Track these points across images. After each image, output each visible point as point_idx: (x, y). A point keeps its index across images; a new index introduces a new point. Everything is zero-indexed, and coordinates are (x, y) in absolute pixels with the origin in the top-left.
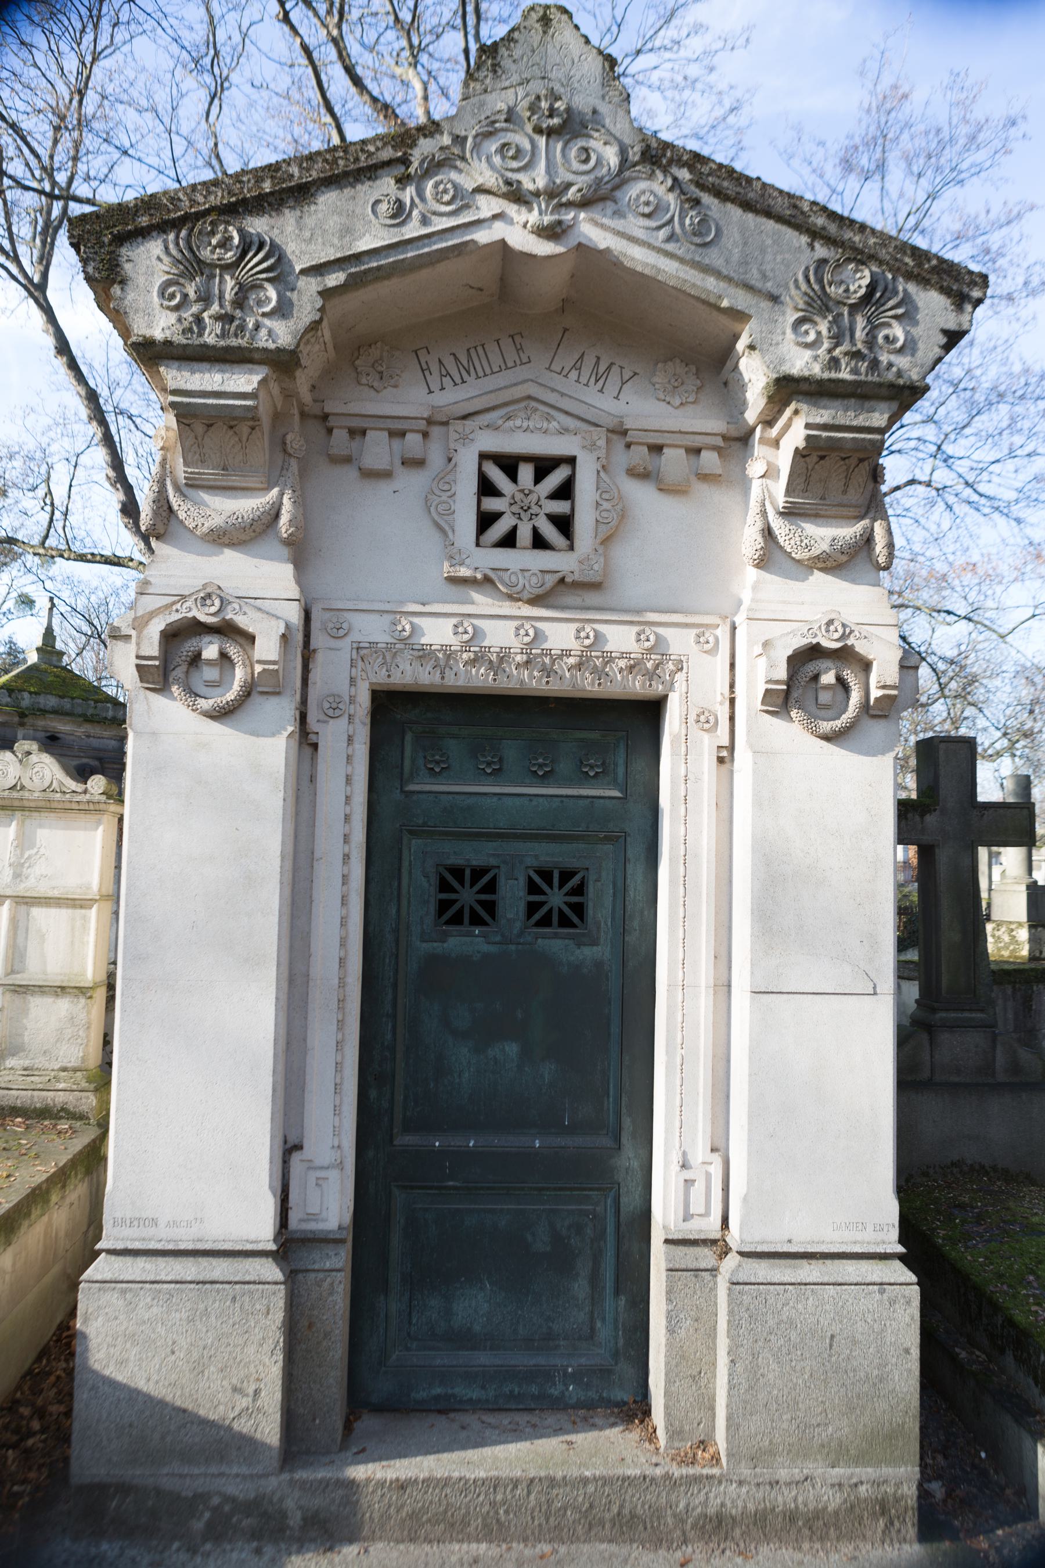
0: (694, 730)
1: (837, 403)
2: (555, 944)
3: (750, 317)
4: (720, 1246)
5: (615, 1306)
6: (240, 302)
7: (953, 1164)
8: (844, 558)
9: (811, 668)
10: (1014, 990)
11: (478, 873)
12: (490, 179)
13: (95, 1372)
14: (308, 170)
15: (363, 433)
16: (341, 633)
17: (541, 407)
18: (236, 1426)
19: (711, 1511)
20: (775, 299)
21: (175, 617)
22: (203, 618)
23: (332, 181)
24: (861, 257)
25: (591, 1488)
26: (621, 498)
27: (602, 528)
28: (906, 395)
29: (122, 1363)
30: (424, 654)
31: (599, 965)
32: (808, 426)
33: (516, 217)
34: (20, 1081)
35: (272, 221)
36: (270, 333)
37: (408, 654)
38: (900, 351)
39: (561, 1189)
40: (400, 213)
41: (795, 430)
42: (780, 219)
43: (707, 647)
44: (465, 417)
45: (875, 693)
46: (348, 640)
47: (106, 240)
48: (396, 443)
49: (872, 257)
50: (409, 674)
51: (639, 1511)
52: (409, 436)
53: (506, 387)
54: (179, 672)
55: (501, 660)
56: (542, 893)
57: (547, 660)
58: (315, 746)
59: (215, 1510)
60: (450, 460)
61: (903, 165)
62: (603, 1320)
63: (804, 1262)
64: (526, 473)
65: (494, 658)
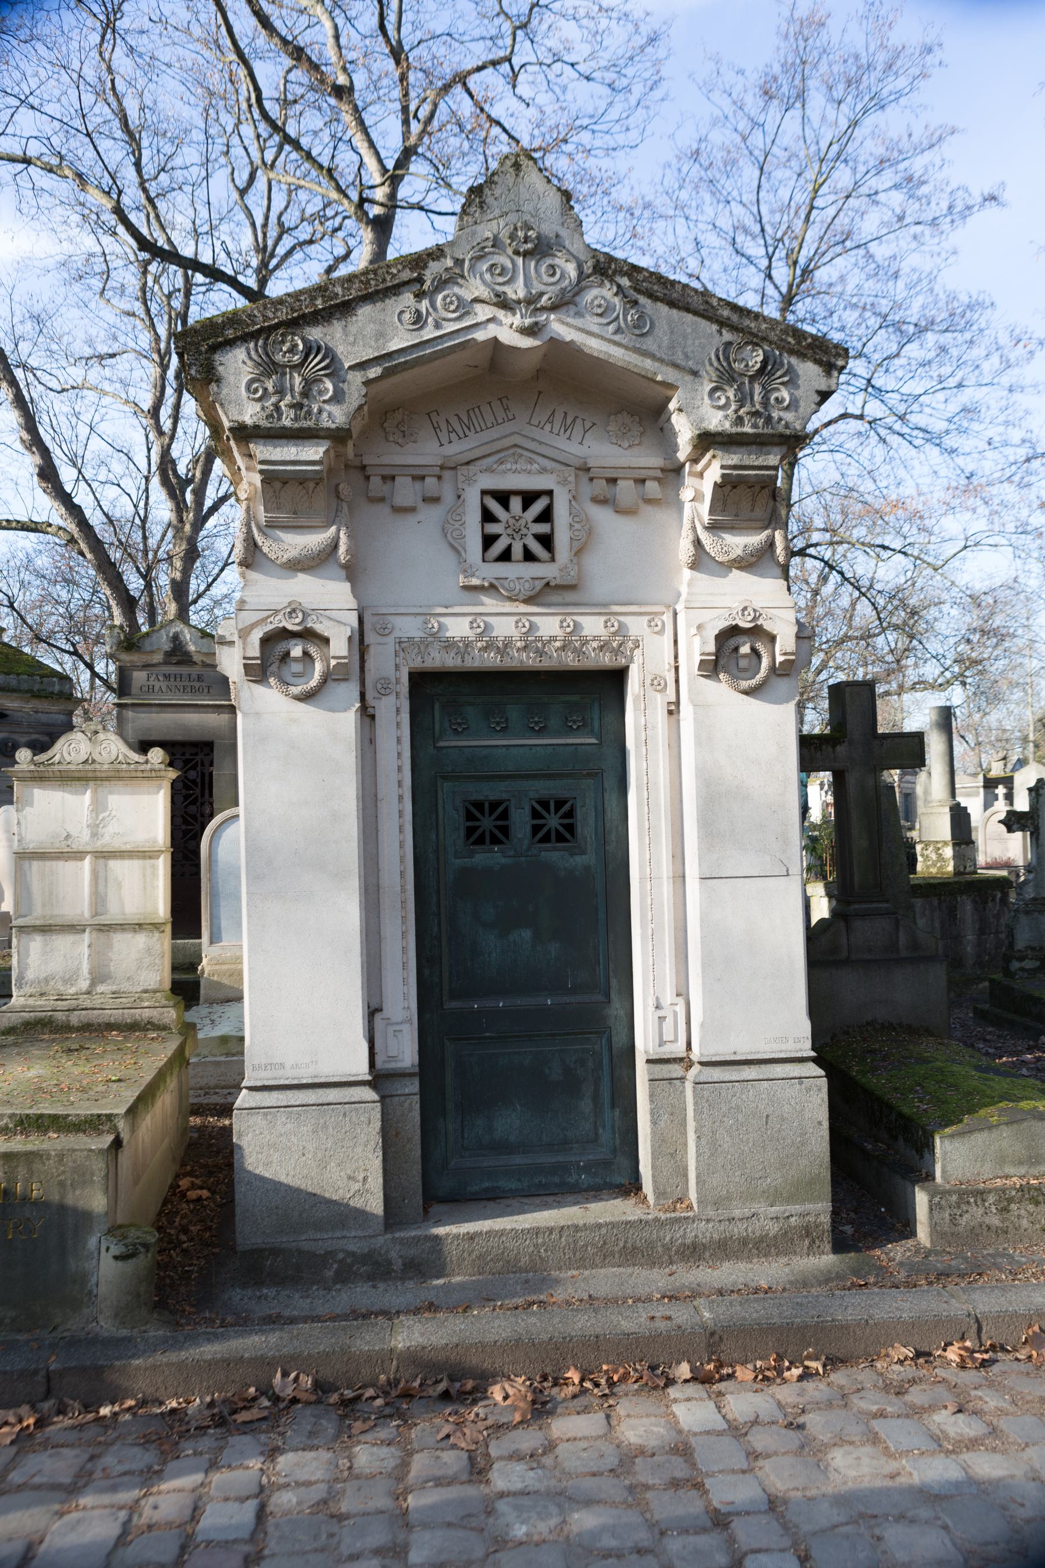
0: (650, 692)
1: (743, 449)
2: (555, 856)
3: (677, 388)
4: (685, 1062)
5: (612, 1116)
6: (306, 393)
7: (868, 1023)
8: (754, 559)
9: (732, 642)
10: (940, 903)
11: (494, 805)
12: (483, 292)
13: (249, 1172)
14: (349, 289)
15: (393, 478)
16: (387, 631)
17: (525, 453)
18: (351, 1203)
19: (688, 1241)
20: (695, 373)
21: (270, 627)
22: (290, 627)
23: (368, 298)
24: (755, 340)
25: (604, 1231)
26: (587, 520)
27: (575, 543)
28: (793, 443)
29: (268, 1164)
30: (449, 645)
31: (587, 868)
32: (723, 467)
33: (504, 320)
34: (110, 1003)
35: (325, 330)
36: (330, 415)
37: (437, 645)
38: (787, 408)
39: (568, 1034)
40: (419, 320)
41: (714, 469)
42: (696, 313)
43: (657, 629)
44: (468, 463)
45: (779, 659)
46: (392, 636)
47: (203, 349)
48: (418, 485)
49: (764, 339)
50: (438, 660)
51: (638, 1244)
52: (428, 480)
53: (498, 439)
54: (274, 668)
55: (506, 646)
56: (542, 817)
57: (540, 645)
58: (373, 717)
59: (341, 1261)
60: (459, 497)
61: (824, 89)
62: (604, 1127)
63: (746, 1067)
64: (516, 503)
65: (500, 645)
